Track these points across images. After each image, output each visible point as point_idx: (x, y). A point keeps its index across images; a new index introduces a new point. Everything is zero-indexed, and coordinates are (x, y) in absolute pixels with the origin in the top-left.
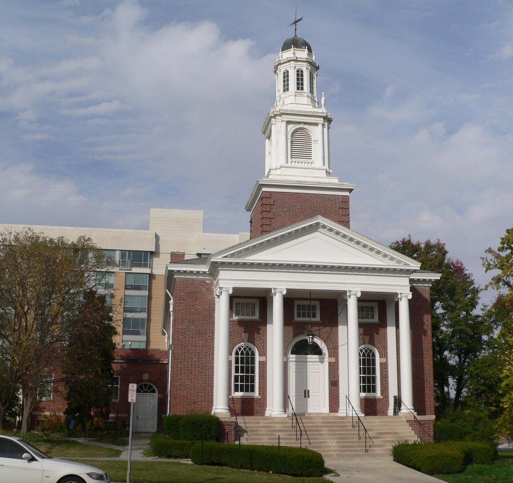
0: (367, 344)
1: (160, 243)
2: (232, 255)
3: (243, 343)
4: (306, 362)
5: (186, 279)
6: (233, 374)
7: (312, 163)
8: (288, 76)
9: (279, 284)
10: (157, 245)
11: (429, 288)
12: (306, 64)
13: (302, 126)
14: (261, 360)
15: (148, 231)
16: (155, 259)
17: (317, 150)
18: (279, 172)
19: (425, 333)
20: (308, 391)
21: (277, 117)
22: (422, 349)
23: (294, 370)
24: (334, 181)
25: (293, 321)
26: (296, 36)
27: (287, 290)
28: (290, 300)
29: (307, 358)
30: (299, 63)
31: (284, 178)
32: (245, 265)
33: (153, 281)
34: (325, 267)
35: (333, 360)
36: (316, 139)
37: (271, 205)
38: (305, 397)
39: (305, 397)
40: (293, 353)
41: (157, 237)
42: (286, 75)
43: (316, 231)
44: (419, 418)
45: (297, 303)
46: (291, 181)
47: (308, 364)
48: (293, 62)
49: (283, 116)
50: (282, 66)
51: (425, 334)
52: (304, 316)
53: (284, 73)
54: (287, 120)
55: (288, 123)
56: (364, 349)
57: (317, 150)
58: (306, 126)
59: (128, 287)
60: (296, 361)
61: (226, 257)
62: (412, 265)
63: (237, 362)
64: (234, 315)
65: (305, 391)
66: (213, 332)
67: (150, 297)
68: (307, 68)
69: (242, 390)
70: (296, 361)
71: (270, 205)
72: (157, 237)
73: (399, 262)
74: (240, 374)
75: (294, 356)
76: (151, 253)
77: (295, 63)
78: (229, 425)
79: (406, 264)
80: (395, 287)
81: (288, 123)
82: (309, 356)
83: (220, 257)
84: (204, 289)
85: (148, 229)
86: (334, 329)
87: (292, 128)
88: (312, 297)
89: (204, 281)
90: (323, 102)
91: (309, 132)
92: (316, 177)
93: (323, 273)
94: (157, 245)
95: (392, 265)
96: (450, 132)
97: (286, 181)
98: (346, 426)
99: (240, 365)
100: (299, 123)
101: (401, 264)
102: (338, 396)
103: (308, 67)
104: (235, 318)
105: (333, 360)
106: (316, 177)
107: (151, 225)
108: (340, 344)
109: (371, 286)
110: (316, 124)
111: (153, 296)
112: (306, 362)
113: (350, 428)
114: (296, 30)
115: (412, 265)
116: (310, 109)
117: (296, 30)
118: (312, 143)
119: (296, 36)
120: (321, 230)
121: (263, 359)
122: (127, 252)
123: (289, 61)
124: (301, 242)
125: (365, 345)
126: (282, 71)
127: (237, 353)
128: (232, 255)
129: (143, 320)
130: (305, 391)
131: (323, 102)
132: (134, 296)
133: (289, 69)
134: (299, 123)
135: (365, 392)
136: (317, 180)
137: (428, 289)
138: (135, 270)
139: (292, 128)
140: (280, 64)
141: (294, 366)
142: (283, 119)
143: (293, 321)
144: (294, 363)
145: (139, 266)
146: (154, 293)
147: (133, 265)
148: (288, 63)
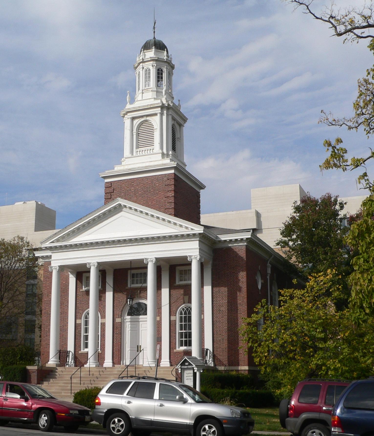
0: (186, 303)
1: (262, 219)
2: (58, 240)
3: (184, 305)
4: (139, 322)
6: (178, 330)
7: (153, 149)
9: (92, 258)
10: (259, 221)
11: (245, 247)
12: (152, 62)
14: (102, 322)
15: (249, 211)
19: (240, 289)
20: (140, 346)
22: (237, 304)
23: (129, 329)
25: (127, 288)
26: (154, 38)
27: (59, 266)
28: (103, 270)
29: (139, 319)
30: (146, 63)
32: (71, 246)
34: (86, 244)
37: (112, 193)
38: (138, 351)
39: (138, 351)
40: (128, 315)
41: (258, 215)
43: (122, 211)
45: (178, 269)
46: (124, 170)
47: (140, 323)
49: (128, 114)
51: (240, 290)
52: (137, 283)
54: (131, 116)
55: (133, 119)
56: (185, 308)
58: (148, 118)
60: (130, 322)
61: (53, 242)
62: (196, 229)
63: (181, 321)
64: (83, 287)
65: (138, 346)
68: (153, 66)
69: (186, 345)
70: (130, 322)
71: (110, 193)
72: (258, 215)
73: (187, 228)
74: (183, 331)
75: (129, 317)
77: (143, 64)
78: (33, 372)
81: (133, 119)
82: (141, 317)
83: (47, 243)
85: (250, 208)
88: (132, 267)
91: (152, 123)
92: (151, 161)
93: (126, 246)
94: (259, 221)
95: (185, 232)
100: (142, 117)
103: (154, 64)
106: (151, 161)
107: (252, 204)
108: (162, 305)
110: (156, 114)
112: (139, 322)
114: (154, 32)
115: (196, 229)
117: (154, 32)
119: (154, 38)
120: (124, 209)
121: (103, 321)
124: (111, 222)
125: (186, 304)
127: (181, 313)
128: (58, 240)
130: (138, 346)
134: (142, 117)
135: (187, 346)
137: (244, 249)
139: (137, 122)
141: (130, 325)
143: (127, 288)
144: (129, 323)
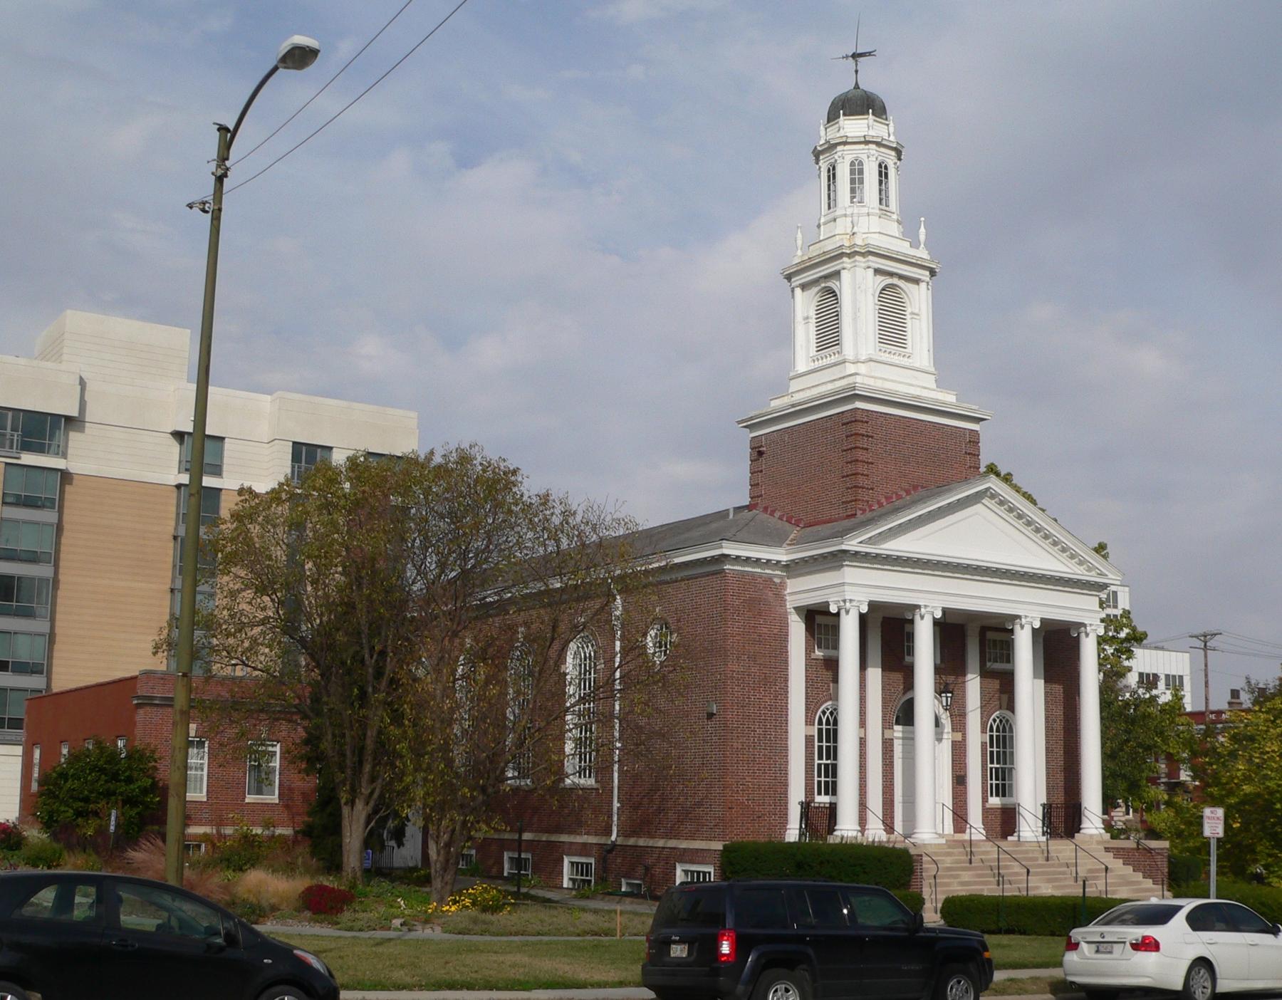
5: (743, 573)
8: (861, 172)
9: (931, 598)
13: (895, 281)
16: (73, 435)
17: (919, 331)
18: (862, 368)
21: (857, 258)
24: (948, 399)
31: (879, 384)
33: (68, 488)
35: (959, 737)
36: (916, 311)
42: (857, 171)
44: (959, 836)
48: (873, 146)
49: (871, 258)
50: (847, 147)
53: (852, 164)
54: (877, 266)
55: (878, 271)
57: (919, 331)
59: (8, 500)
62: (1110, 576)
66: (786, 680)
67: (59, 528)
72: (82, 383)
76: (69, 419)
79: (1102, 574)
80: (1081, 613)
83: (854, 542)
84: (770, 594)
86: (960, 680)
87: (883, 281)
89: (769, 579)
90: (922, 237)
96: (465, 161)
97: (895, 393)
98: (1036, 859)
99: (824, 744)
100: (891, 274)
101: (1093, 573)
102: (892, 801)
104: (818, 653)
105: (959, 737)
109: (882, 591)
110: (916, 281)
111: (66, 526)
113: (1041, 861)
114: (857, 72)
115: (1110, 576)
116: (904, 248)
117: (857, 72)
118: (908, 317)
122: (10, 414)
123: (867, 143)
126: (849, 159)
129: (42, 580)
131: (922, 237)
132: (25, 522)
133: (864, 157)
134: (891, 274)
136: (917, 392)
138: (28, 459)
140: (845, 143)
142: (870, 264)
145: (41, 449)
146: (66, 518)
147: (26, 447)
148: (862, 146)
